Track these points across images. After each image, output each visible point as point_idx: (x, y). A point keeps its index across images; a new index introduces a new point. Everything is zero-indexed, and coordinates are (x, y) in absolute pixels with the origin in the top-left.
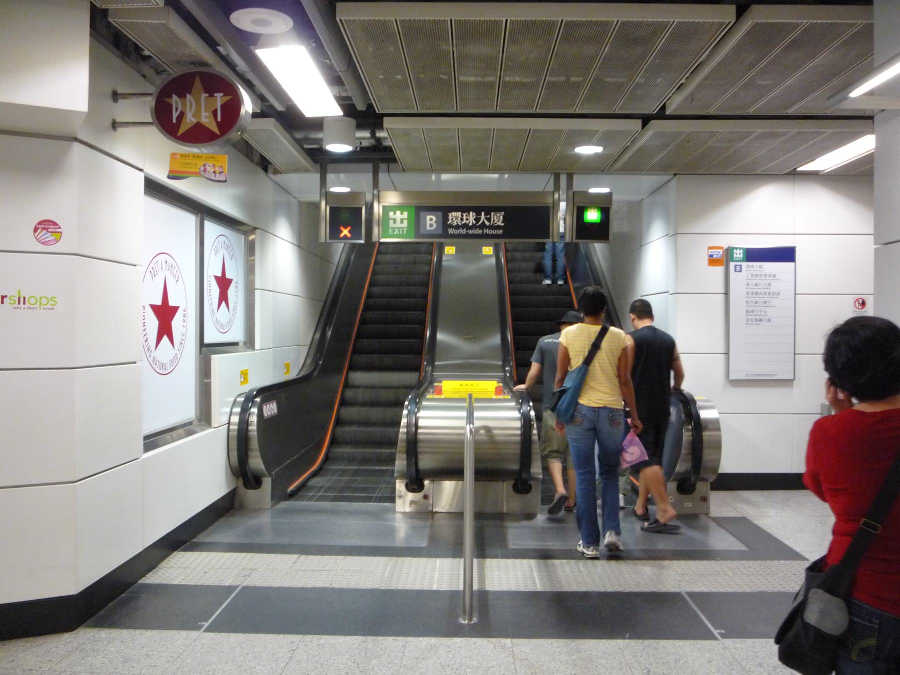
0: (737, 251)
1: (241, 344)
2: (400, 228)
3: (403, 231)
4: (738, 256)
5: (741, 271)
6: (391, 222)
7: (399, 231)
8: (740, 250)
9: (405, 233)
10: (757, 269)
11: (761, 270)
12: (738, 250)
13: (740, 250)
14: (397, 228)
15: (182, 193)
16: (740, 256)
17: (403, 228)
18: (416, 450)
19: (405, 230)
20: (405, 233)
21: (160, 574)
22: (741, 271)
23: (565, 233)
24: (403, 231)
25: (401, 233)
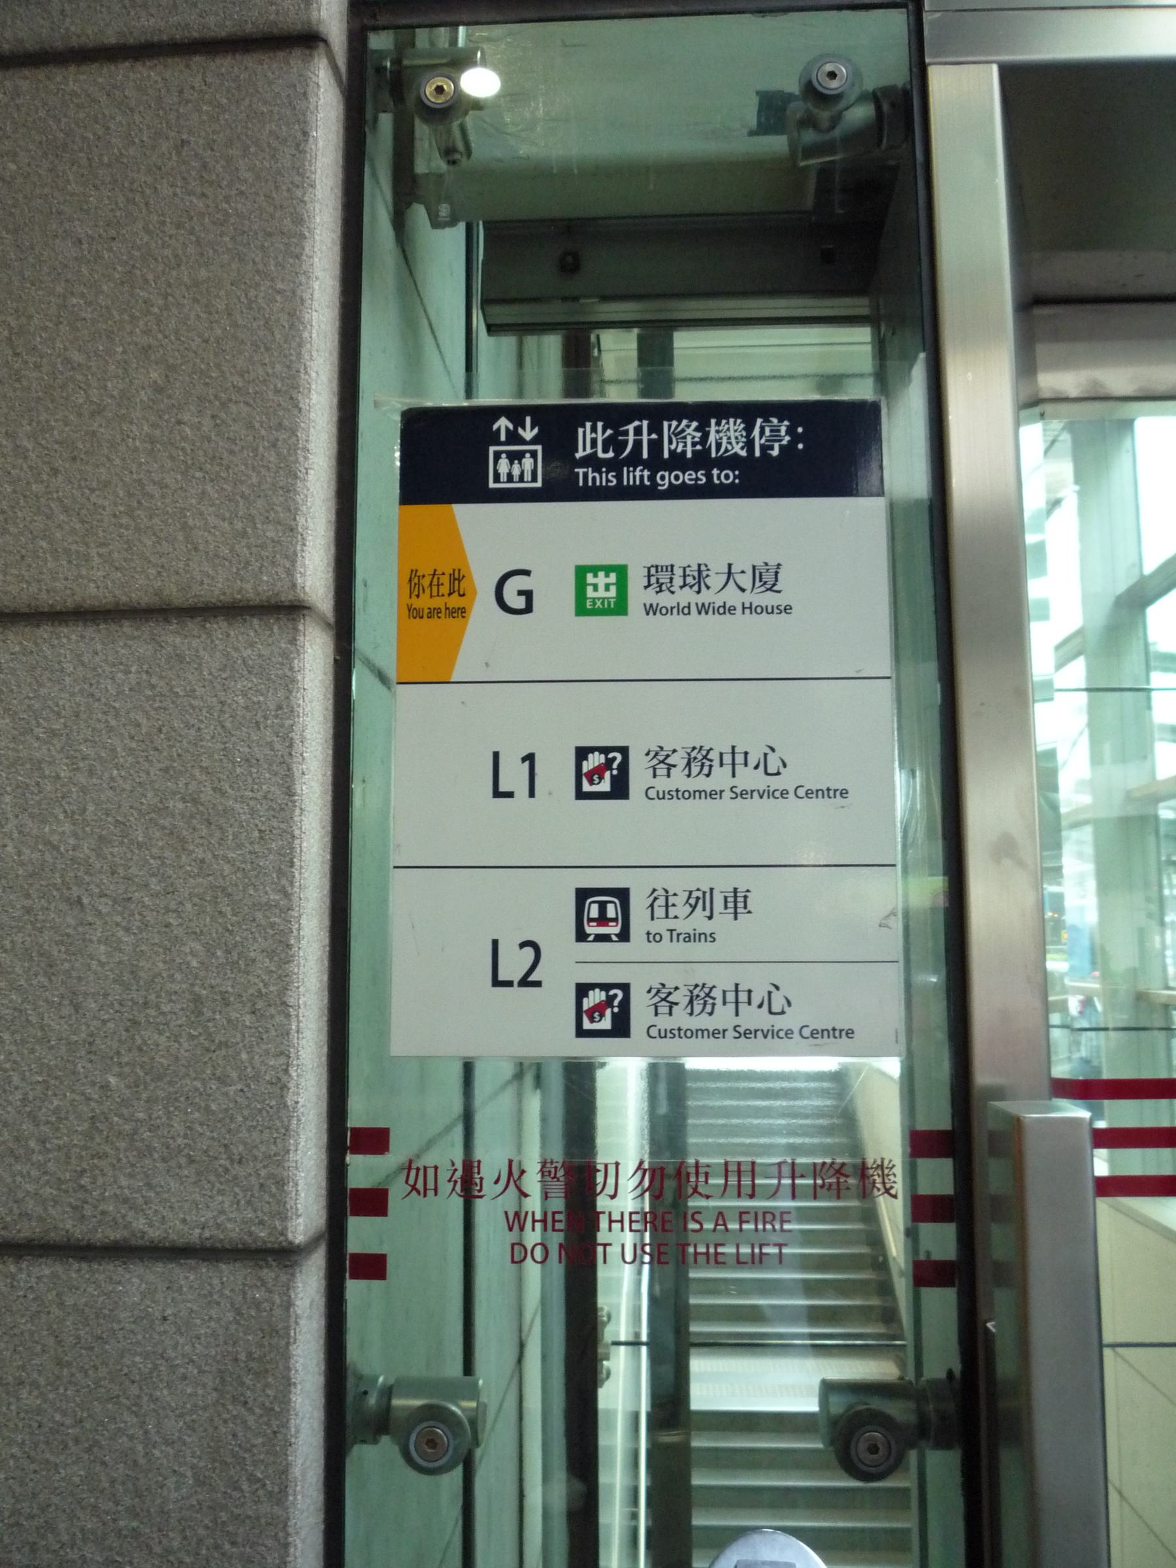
0: (596, 576)
1: (516, 984)
2: (604, 599)
3: (609, 603)
4: (601, 593)
5: (689, 613)
6: (590, 589)
7: (603, 603)
8: (607, 576)
9: (612, 606)
10: (732, 596)
11: (769, 599)
12: (601, 574)
13: (607, 576)
14: (599, 599)
15: (927, 413)
16: (607, 595)
17: (608, 598)
18: (185, 44)
19: (612, 600)
20: (612, 606)
21: (322, 551)
22: (689, 613)
23: (1017, 424)
24: (609, 603)
25: (606, 606)
